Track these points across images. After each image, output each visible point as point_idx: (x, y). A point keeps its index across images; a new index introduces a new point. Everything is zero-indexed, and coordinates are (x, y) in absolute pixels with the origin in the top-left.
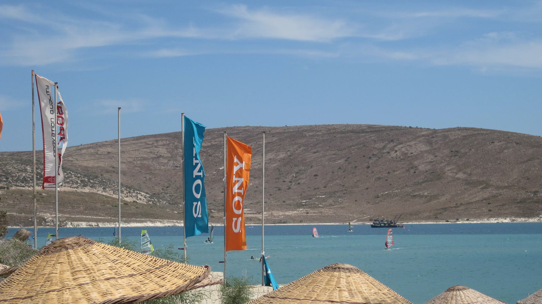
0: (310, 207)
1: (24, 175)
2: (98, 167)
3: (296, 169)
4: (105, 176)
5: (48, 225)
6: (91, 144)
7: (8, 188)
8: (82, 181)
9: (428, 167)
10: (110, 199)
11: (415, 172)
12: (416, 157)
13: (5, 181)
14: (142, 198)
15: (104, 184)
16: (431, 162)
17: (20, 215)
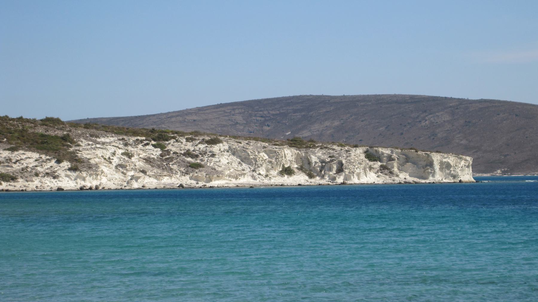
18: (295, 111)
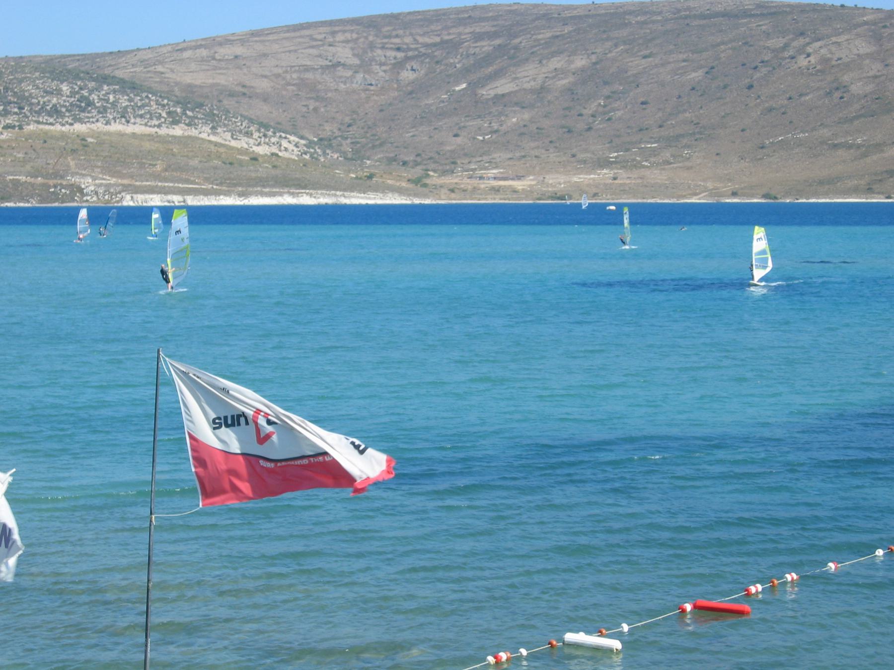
0: (624, 167)
1: (54, 100)
2: (213, 85)
3: (606, 91)
4: (225, 102)
5: (87, 201)
6: (203, 40)
7: (21, 128)
8: (169, 113)
9: (870, 88)
10: (222, 150)
11: (841, 98)
12: (847, 67)
13: (16, 113)
14: (291, 147)
15: (214, 121)
16: (876, 77)
17: (32, 180)
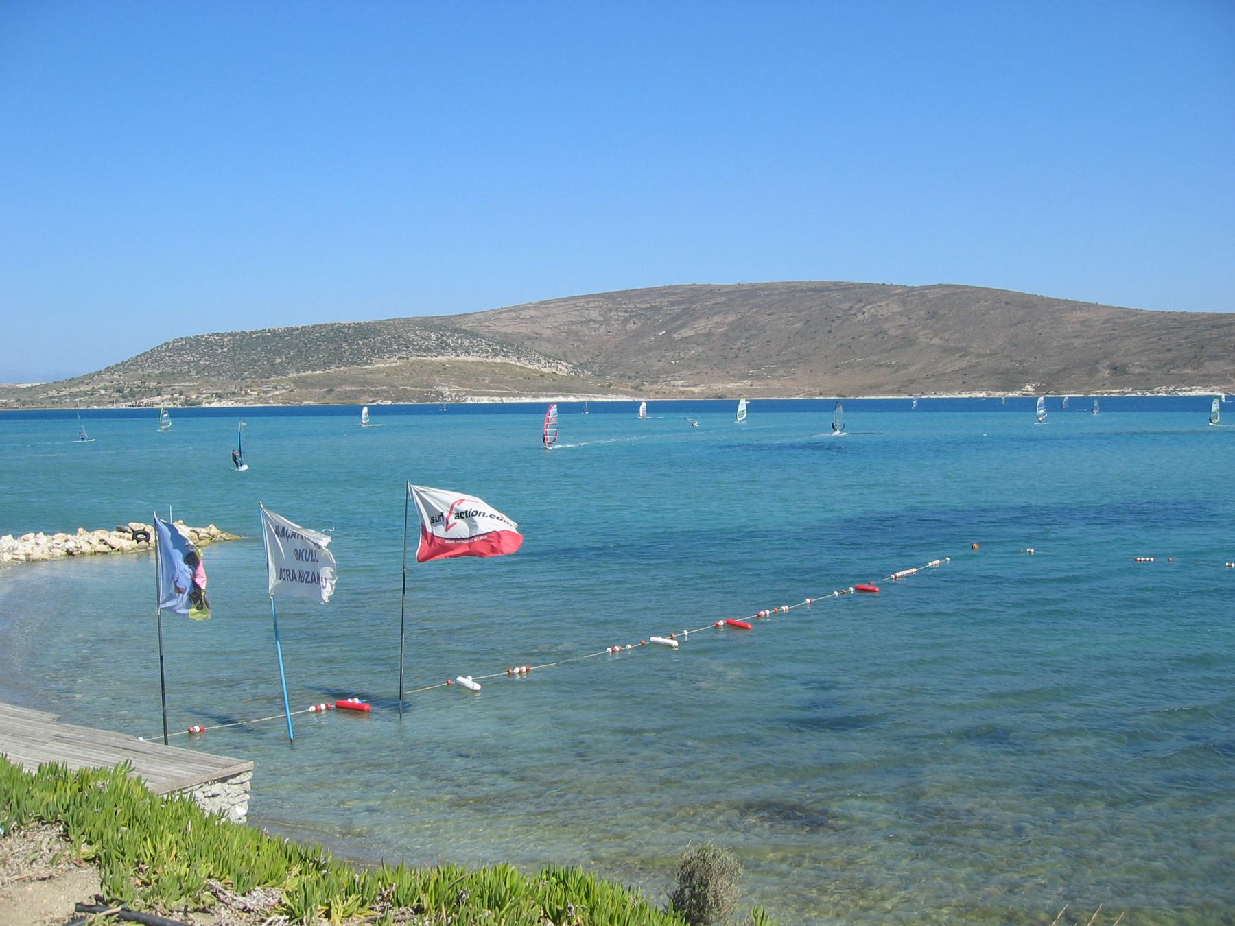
3: (746, 334)
9: (899, 332)
12: (886, 320)
15: (518, 354)
18: (672, 304)
